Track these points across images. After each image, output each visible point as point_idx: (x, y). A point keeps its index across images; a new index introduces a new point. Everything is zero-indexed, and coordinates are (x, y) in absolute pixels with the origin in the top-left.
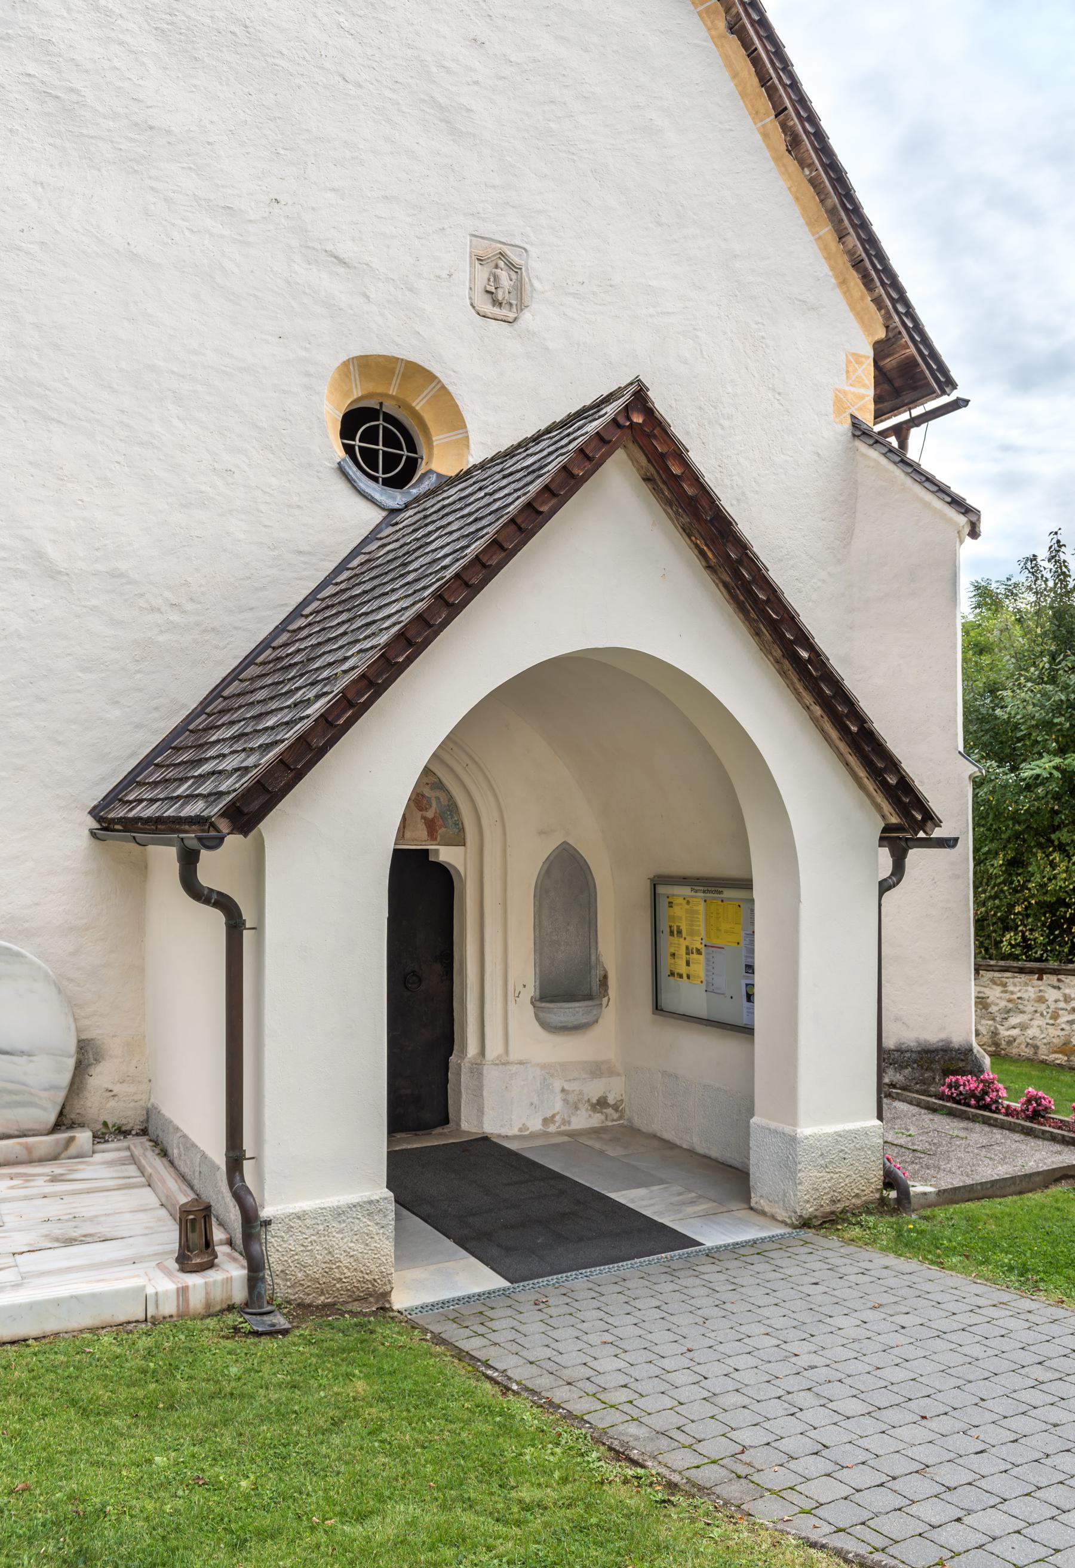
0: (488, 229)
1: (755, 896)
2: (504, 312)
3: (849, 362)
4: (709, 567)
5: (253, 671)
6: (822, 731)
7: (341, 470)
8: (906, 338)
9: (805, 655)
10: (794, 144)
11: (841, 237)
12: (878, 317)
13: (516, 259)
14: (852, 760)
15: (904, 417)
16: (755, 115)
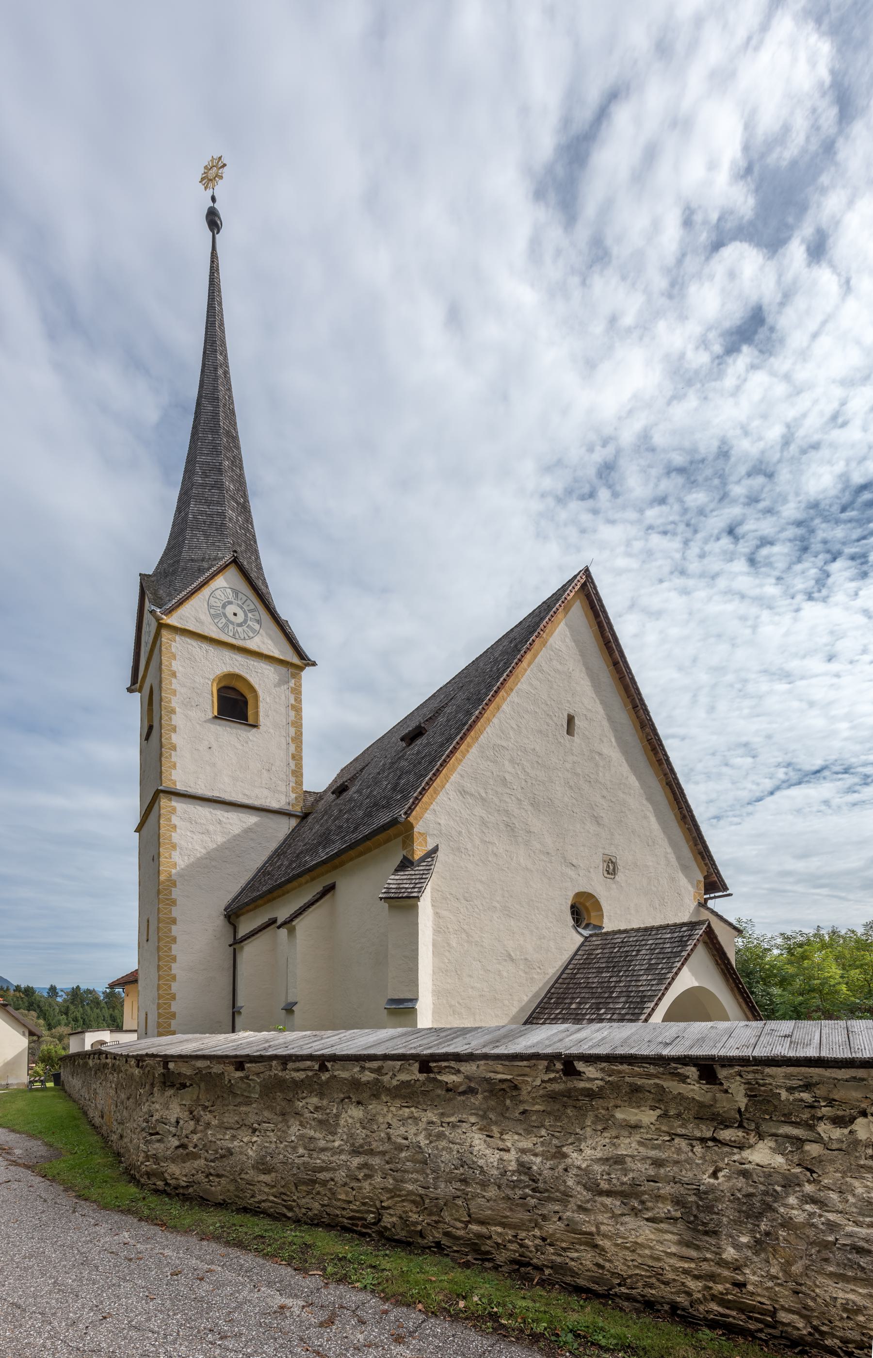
0: (607, 852)
5: (557, 985)
10: (684, 817)
11: (696, 845)
12: (705, 868)
13: (614, 860)
16: (673, 810)
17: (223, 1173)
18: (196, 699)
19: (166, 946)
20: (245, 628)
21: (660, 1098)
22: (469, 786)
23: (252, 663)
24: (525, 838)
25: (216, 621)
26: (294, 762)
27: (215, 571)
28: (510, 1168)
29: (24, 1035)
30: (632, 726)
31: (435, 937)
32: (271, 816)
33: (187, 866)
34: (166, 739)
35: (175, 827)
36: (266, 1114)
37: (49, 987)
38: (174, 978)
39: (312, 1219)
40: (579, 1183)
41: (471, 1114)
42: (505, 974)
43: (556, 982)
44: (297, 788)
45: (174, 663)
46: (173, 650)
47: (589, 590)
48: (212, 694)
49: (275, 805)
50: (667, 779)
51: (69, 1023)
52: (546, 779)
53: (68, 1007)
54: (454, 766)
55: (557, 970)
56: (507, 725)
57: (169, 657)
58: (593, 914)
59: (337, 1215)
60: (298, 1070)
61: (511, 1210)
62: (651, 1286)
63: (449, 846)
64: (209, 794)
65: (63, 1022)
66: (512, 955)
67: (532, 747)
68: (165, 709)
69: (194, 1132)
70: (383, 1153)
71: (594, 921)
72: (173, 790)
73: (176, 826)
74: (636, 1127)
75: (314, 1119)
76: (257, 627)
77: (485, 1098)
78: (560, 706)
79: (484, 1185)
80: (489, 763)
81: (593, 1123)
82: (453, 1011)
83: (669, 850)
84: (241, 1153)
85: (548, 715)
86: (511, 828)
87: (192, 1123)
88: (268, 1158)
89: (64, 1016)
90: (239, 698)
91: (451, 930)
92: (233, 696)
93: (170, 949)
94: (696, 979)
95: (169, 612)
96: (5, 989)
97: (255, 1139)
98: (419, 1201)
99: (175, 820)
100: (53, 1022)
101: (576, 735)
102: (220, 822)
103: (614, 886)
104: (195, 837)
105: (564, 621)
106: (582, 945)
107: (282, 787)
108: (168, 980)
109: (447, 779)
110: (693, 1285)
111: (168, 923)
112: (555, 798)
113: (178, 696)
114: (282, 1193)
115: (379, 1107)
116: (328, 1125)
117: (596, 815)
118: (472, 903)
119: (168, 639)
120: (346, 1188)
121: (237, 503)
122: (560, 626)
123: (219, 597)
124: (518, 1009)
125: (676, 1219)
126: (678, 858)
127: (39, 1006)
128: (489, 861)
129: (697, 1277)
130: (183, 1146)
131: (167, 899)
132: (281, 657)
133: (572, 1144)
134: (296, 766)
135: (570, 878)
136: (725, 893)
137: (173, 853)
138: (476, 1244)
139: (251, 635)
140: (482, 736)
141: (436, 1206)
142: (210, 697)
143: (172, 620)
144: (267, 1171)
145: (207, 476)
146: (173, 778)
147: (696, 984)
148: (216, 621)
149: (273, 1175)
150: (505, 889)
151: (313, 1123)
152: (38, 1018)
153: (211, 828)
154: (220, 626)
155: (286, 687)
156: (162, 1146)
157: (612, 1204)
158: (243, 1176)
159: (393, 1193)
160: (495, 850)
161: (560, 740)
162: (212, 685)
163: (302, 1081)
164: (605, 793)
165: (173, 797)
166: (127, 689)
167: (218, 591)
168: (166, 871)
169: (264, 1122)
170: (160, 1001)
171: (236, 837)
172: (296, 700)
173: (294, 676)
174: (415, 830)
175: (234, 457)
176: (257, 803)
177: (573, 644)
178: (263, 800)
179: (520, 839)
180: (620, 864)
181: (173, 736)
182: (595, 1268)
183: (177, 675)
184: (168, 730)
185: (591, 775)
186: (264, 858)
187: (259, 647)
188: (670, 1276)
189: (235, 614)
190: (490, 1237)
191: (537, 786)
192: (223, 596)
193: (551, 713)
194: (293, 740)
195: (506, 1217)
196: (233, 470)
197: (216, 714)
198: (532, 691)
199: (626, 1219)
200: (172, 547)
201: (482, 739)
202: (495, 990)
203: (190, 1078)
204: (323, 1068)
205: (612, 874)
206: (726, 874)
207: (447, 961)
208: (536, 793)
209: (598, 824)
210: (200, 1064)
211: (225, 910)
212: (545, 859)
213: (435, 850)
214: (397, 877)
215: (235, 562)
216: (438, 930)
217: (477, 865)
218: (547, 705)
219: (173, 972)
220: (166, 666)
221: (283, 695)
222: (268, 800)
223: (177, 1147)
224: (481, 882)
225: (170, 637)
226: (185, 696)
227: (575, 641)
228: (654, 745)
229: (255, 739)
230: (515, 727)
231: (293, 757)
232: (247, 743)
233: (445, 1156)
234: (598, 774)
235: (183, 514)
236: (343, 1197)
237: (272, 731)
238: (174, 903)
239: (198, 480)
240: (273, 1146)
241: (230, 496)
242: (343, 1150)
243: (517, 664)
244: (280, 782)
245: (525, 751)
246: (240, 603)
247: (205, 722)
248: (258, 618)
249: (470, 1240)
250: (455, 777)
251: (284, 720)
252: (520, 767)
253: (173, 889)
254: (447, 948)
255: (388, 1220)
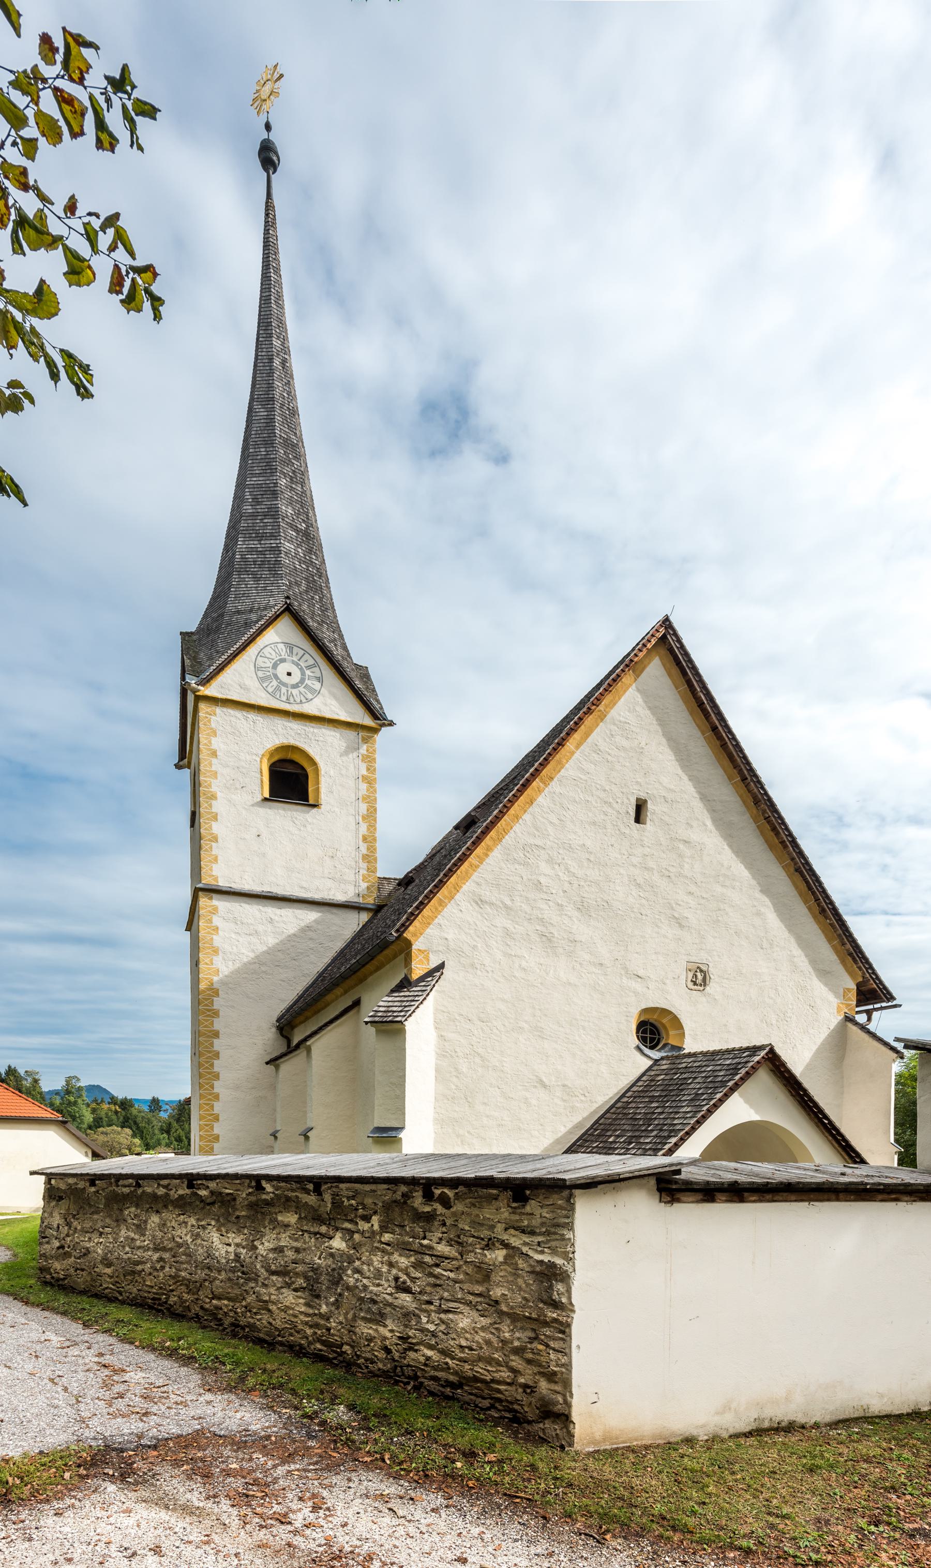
0: (693, 959)
1: (22, 291)
2: (699, 988)
3: (844, 992)
4: (792, 1095)
5: (608, 1115)
6: (832, 1144)
7: (638, 1048)
8: (872, 982)
9: (826, 1122)
10: (823, 911)
11: (843, 944)
13: (704, 968)
14: (843, 1153)
15: (871, 1007)
16: (806, 902)
17: (84, 1267)
18: (241, 780)
19: (207, 1062)
20: (302, 689)
21: (298, 1206)
22: (487, 893)
23: (312, 730)
24: (567, 948)
25: (265, 685)
26: (365, 845)
27: (262, 625)
28: (231, 1258)
29: (87, 1155)
30: (741, 802)
31: (439, 1062)
32: (335, 910)
33: (232, 973)
34: (205, 829)
35: (217, 929)
36: (108, 1221)
37: (151, 1098)
38: (217, 1097)
39: (132, 1301)
40: (262, 1267)
41: (212, 1219)
42: (534, 1102)
43: (607, 1111)
44: (369, 876)
45: (214, 740)
46: (213, 725)
47: (671, 644)
48: (261, 772)
49: (340, 898)
50: (796, 864)
51: (171, 1143)
52: (600, 878)
53: (170, 1124)
54: (467, 873)
55: (611, 1098)
56: (544, 820)
57: (208, 734)
58: (671, 1033)
59: (145, 1297)
60: (125, 1186)
61: (232, 1288)
62: (291, 1335)
63: (460, 962)
64: (257, 888)
65: (163, 1142)
66: (544, 1079)
67: (581, 843)
68: (204, 794)
69: (68, 1235)
70: (171, 1249)
71: (672, 1041)
72: (214, 887)
73: (217, 928)
74: (287, 1226)
75: (134, 1224)
76: (317, 686)
77: (220, 1207)
78: (624, 790)
79: (219, 1271)
80: (517, 866)
81: (269, 1223)
82: (462, 1141)
83: (797, 952)
84: (94, 1252)
85: (606, 802)
86: (547, 939)
87: (66, 1228)
88: (109, 1255)
89: (165, 1135)
90: (299, 771)
91: (460, 1054)
92: (290, 769)
93: (212, 1065)
94: (757, 1112)
95: (206, 682)
96: (99, 1101)
97: (101, 1240)
98: (187, 1283)
99: (217, 921)
100: (151, 1142)
101: (648, 822)
102: (271, 921)
103: (704, 999)
104: (241, 939)
105: (634, 685)
106: (649, 1069)
107: (350, 876)
108: (209, 1100)
109: (457, 888)
110: (309, 1332)
111: (209, 1037)
112: (613, 899)
113: (219, 778)
114: (117, 1282)
115: (168, 1215)
116: (140, 1229)
117: (677, 916)
118: (489, 1024)
119: (207, 713)
120: (151, 1277)
121: (297, 530)
122: (628, 693)
123: (268, 656)
124: (551, 1141)
125: (304, 1288)
126: (813, 962)
127: (135, 1123)
128: (515, 977)
129: (311, 1327)
130: (62, 1247)
131: (209, 1010)
132: (349, 720)
133: (258, 1239)
134: (368, 849)
135: (634, 992)
136: (890, 1004)
137: (215, 958)
138: (215, 1314)
139: (310, 696)
140: (507, 837)
141: (195, 1287)
142: (259, 776)
143: (210, 690)
144: (109, 1265)
145: (259, 503)
146: (214, 873)
147: (755, 1117)
148: (265, 685)
149: (112, 1268)
150: (537, 1007)
151: (133, 1227)
152: (134, 1136)
153: (260, 928)
154: (270, 690)
155: (355, 754)
156: (49, 1246)
157: (276, 1280)
158: (96, 1269)
159: (174, 1277)
160: (524, 964)
161: (623, 830)
162: (261, 762)
163: (128, 1194)
164: (692, 888)
165: (214, 895)
166: (175, 765)
167: (268, 649)
168: (206, 979)
169: (106, 1227)
170: (201, 1123)
171: (292, 938)
172: (368, 769)
173: (365, 740)
174: (414, 947)
175: (294, 472)
176: (317, 896)
177: (648, 712)
178: (326, 893)
179: (561, 950)
180: (713, 972)
181: (214, 825)
182: (268, 1325)
183: (218, 753)
184: (208, 819)
185: (671, 869)
186: (327, 960)
187: (320, 710)
188: (300, 1327)
189: (289, 674)
190: (221, 1309)
191: (587, 888)
192: (273, 653)
193: (611, 800)
194: (364, 818)
195: (229, 1293)
196: (292, 489)
197: (268, 796)
198: (582, 777)
199: (284, 1290)
200: (218, 597)
201: (508, 839)
202: (520, 1120)
203: (64, 1191)
204: (138, 1185)
205: (701, 985)
206: (888, 975)
207: (454, 1087)
208: (585, 895)
209: (681, 926)
210: (71, 1181)
211: (277, 1021)
212: (597, 971)
213: (442, 966)
214: (390, 999)
215: (288, 609)
216: (445, 1053)
217: (498, 982)
218: (605, 790)
219: (216, 1090)
220: (205, 744)
221: (352, 765)
222: (332, 892)
223: (58, 1248)
224: (503, 1000)
225: (209, 710)
226: (228, 778)
227: (650, 708)
228: (773, 824)
229: (315, 821)
230: (556, 821)
231: (365, 839)
232: (305, 826)
233: (201, 1251)
234: (681, 867)
235: (230, 553)
236: (148, 1283)
237: (337, 810)
238: (216, 1014)
239: (248, 509)
240: (112, 1246)
241: (287, 523)
242: (149, 1248)
243: (554, 749)
244: (347, 870)
245: (570, 848)
246: (295, 659)
247: (253, 805)
248: (319, 675)
249: (212, 1310)
250: (468, 886)
251: (353, 796)
252: (562, 867)
253: (215, 999)
254: (455, 1074)
255: (173, 1299)
